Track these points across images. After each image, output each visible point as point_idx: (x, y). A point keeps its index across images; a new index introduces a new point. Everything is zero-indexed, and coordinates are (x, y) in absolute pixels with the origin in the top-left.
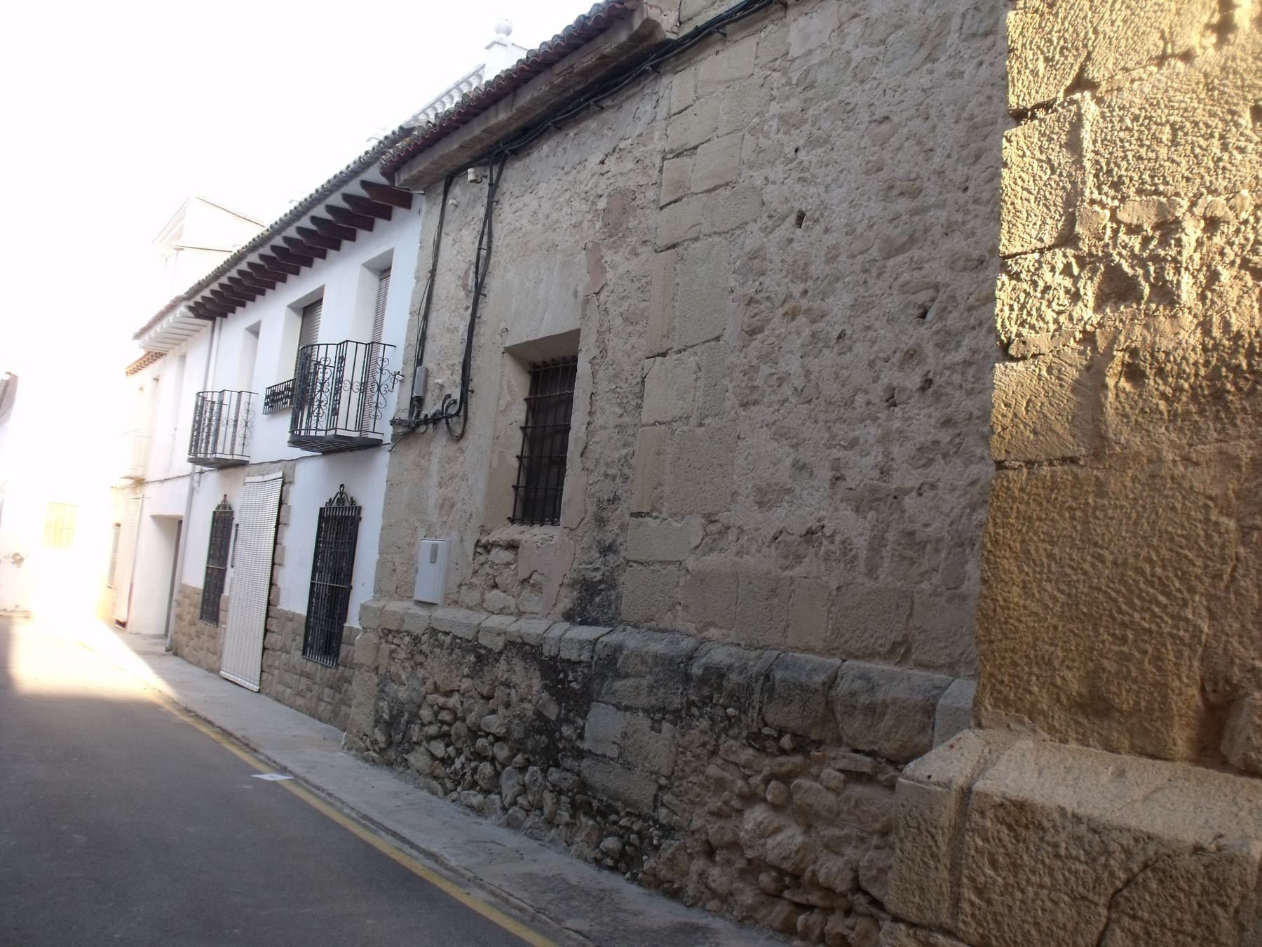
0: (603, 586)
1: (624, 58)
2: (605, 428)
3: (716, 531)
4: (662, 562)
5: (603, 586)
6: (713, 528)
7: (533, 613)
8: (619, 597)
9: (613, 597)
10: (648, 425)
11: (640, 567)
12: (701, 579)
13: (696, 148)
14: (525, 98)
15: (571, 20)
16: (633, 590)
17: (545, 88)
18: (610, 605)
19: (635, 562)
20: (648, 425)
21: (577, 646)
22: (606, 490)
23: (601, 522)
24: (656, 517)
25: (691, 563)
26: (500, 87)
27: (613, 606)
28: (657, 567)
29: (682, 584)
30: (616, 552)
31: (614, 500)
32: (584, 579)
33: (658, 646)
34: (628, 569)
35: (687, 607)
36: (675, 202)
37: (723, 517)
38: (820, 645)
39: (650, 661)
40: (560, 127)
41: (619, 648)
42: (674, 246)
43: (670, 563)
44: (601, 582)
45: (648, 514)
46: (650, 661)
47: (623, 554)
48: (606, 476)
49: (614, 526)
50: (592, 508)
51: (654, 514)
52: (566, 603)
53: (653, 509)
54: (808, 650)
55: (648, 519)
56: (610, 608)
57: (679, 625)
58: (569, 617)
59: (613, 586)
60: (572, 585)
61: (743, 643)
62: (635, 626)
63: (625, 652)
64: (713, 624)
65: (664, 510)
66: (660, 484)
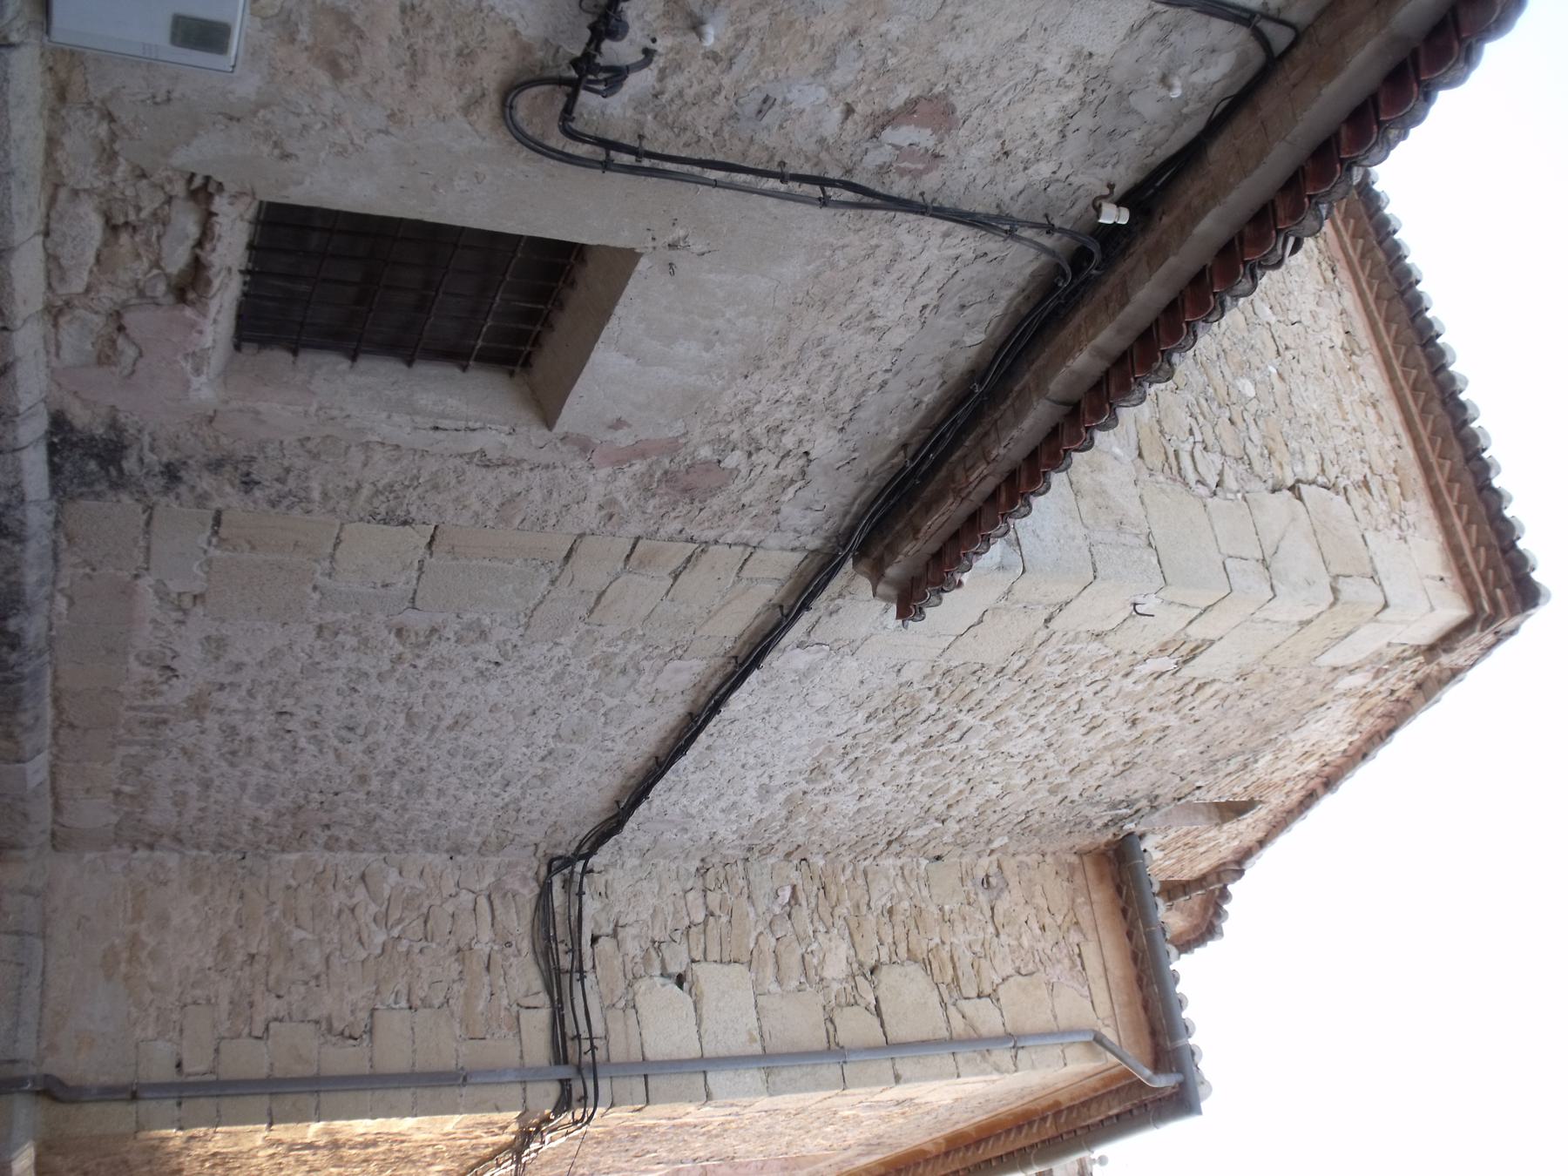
0: (113, 472)
1: (898, 527)
2: (365, 465)
3: (181, 606)
4: (148, 549)
5: (113, 472)
6: (187, 601)
7: (58, 347)
8: (98, 496)
9: (98, 488)
10: (341, 530)
11: (142, 523)
12: (126, 592)
13: (676, 578)
14: (1037, 417)
15: (1394, 154)
16: (110, 515)
17: (998, 451)
18: (85, 484)
19: (150, 518)
20: (341, 530)
21: (12, 481)
22: (265, 471)
23: (215, 466)
24: (209, 543)
25: (146, 583)
26: (1230, 279)
27: (84, 489)
28: (142, 543)
29: (120, 574)
30: (167, 490)
31: (248, 484)
32: (125, 447)
33: (31, 577)
34: (140, 508)
35: (90, 577)
36: (628, 557)
37: (199, 610)
38: (61, 684)
39: (12, 578)
40: (975, 374)
41: (20, 539)
42: (568, 557)
43: (147, 560)
44: (121, 470)
45: (215, 533)
46: (12, 578)
47: (163, 500)
48: (288, 470)
49: (206, 483)
50: (241, 451)
51: (214, 540)
52: (80, 417)
53: (222, 540)
54: (56, 678)
55: (208, 532)
56: (79, 485)
57: (66, 572)
58: (59, 422)
59: (115, 486)
60: (114, 425)
61: (54, 633)
62: (57, 523)
63: (17, 548)
64: (71, 602)
65: (218, 553)
66: (253, 548)
